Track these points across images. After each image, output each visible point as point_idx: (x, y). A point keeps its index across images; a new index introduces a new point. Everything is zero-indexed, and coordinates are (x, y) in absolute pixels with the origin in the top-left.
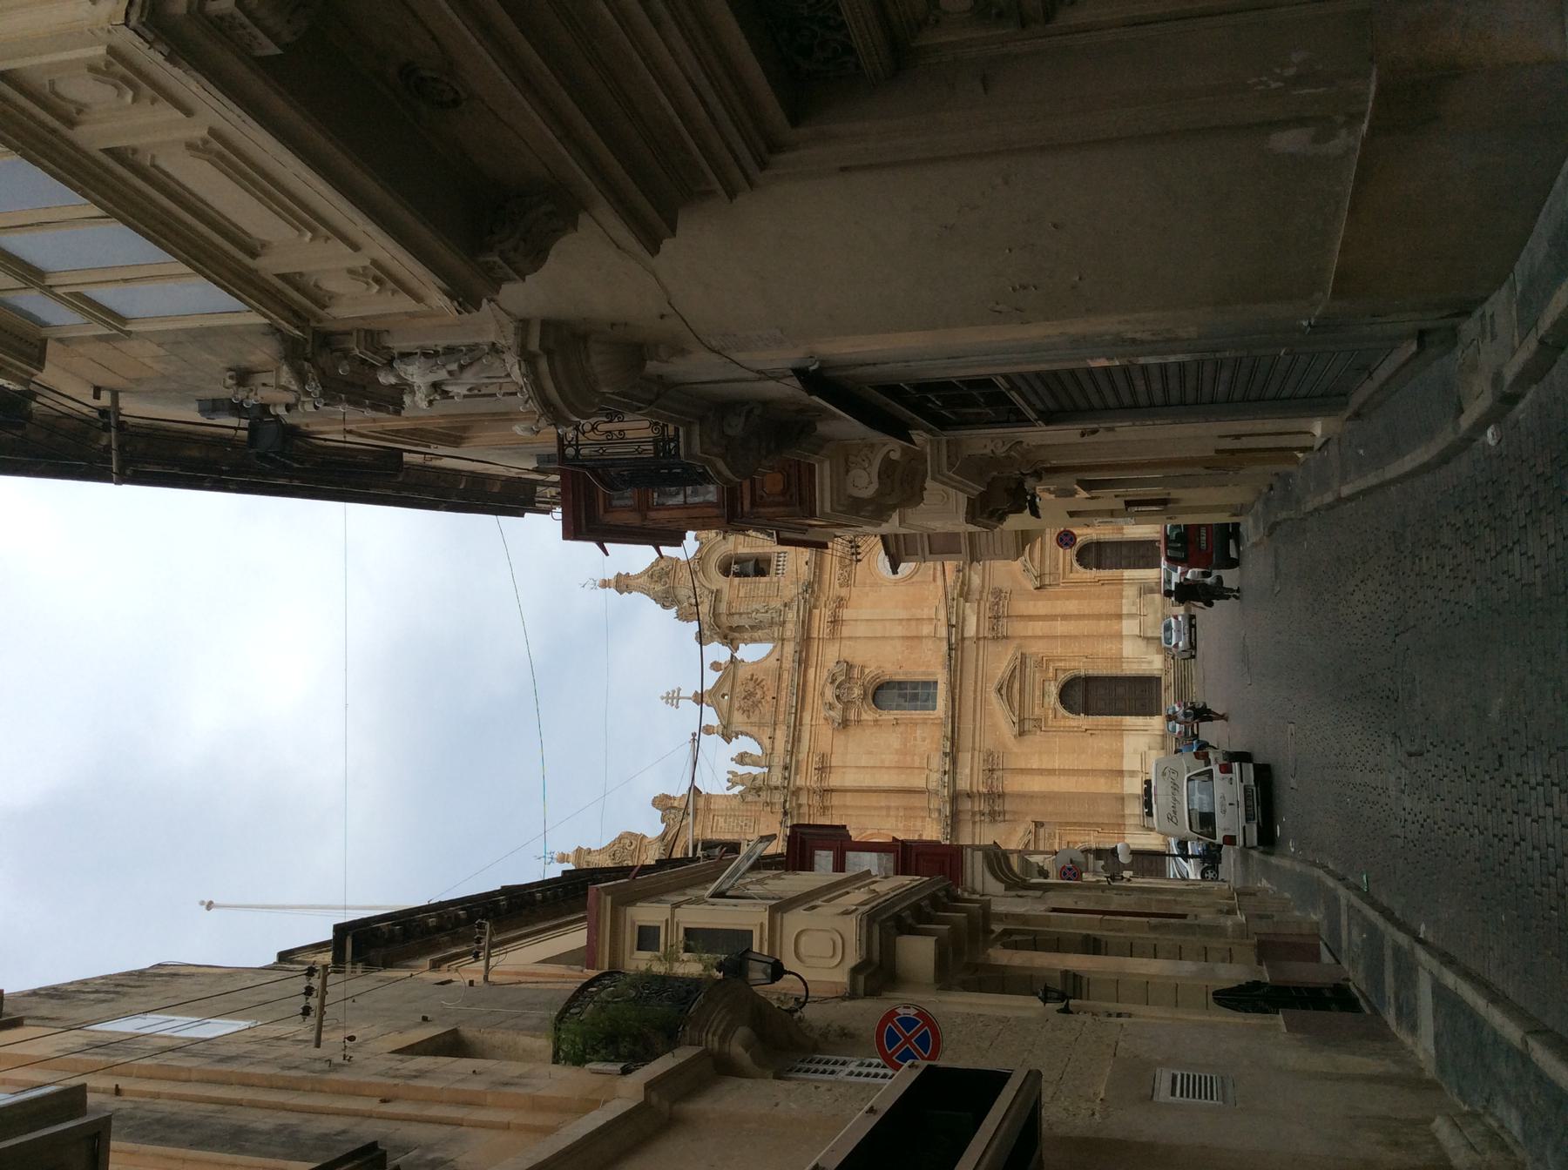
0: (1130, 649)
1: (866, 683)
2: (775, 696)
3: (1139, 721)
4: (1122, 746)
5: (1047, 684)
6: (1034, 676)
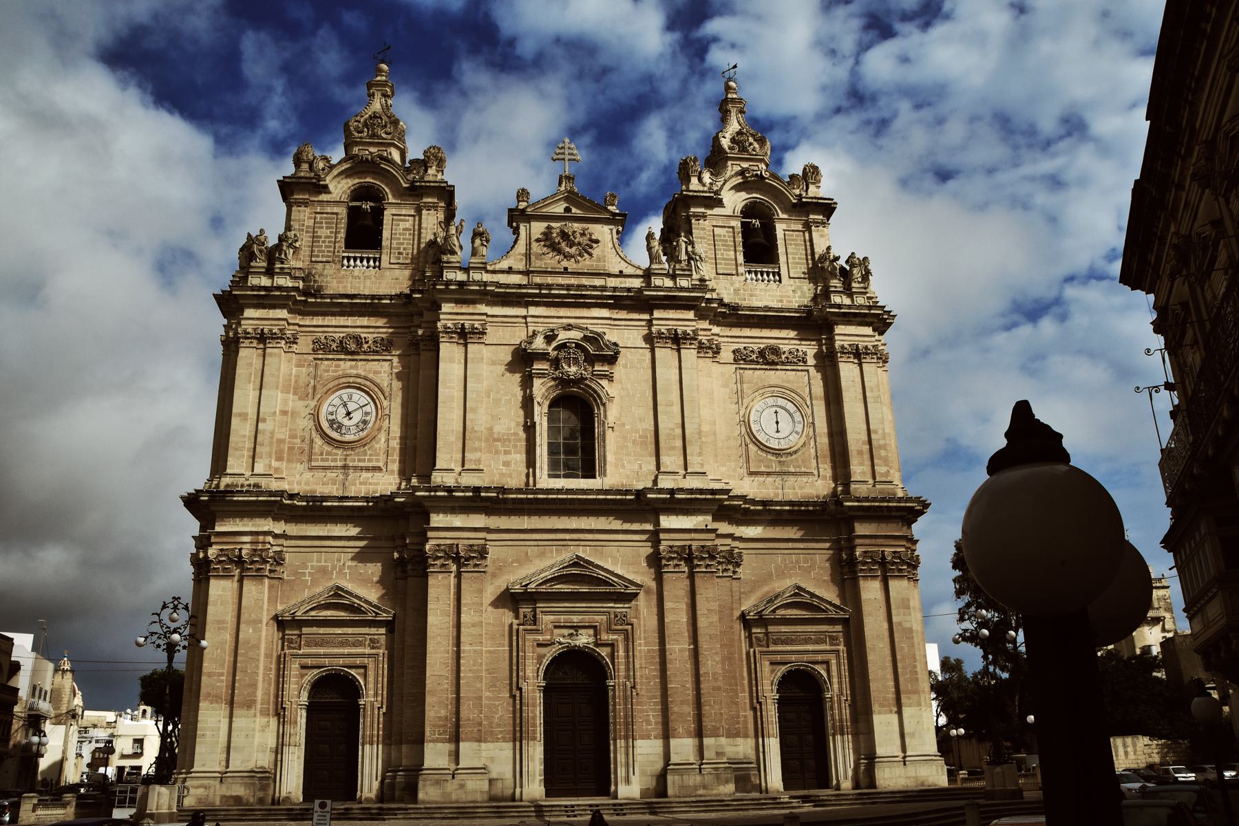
0: (647, 750)
1: (587, 382)
4: (497, 740)
5: (591, 632)
6: (599, 613)
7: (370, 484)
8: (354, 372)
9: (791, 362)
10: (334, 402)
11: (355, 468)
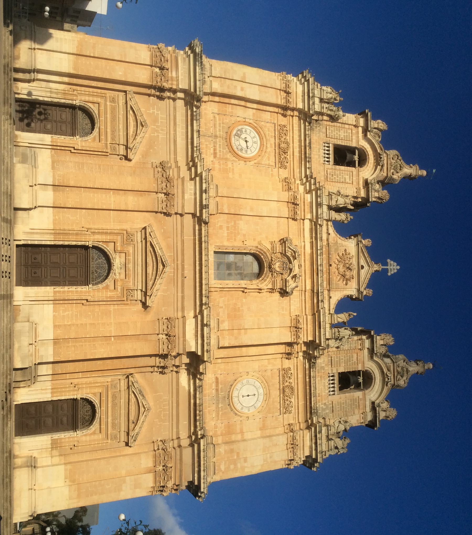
7: (206, 151)
8: (269, 146)
9: (285, 402)
10: (252, 133)
11: (215, 143)
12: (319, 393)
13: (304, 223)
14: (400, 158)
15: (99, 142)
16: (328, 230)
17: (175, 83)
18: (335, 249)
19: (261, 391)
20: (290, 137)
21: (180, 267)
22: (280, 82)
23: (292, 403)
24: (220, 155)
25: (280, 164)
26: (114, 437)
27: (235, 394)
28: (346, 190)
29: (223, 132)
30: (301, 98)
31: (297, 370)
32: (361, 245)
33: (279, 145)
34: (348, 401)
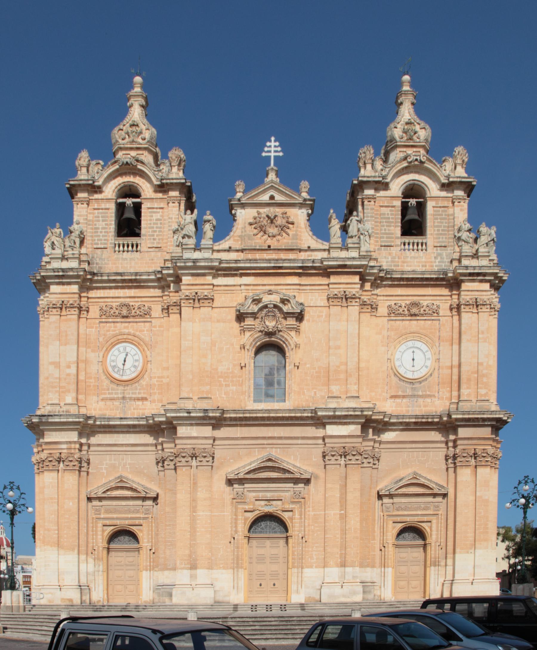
2: (272, 248)
3: (242, 582)
4: (220, 568)
7: (140, 409)
8: (126, 331)
12: (423, 266)
13: (218, 286)
14: (121, 127)
15: (141, 525)
16: (225, 251)
17: (73, 446)
18: (249, 239)
19: (410, 344)
20: (113, 302)
21: (270, 441)
22: (51, 316)
23: (429, 305)
24: (144, 393)
25: (146, 316)
26: (437, 508)
27: (410, 375)
28: (172, 218)
29: (118, 390)
30: (65, 287)
31: (392, 296)
32: (244, 201)
33: (124, 317)
34: (436, 224)
